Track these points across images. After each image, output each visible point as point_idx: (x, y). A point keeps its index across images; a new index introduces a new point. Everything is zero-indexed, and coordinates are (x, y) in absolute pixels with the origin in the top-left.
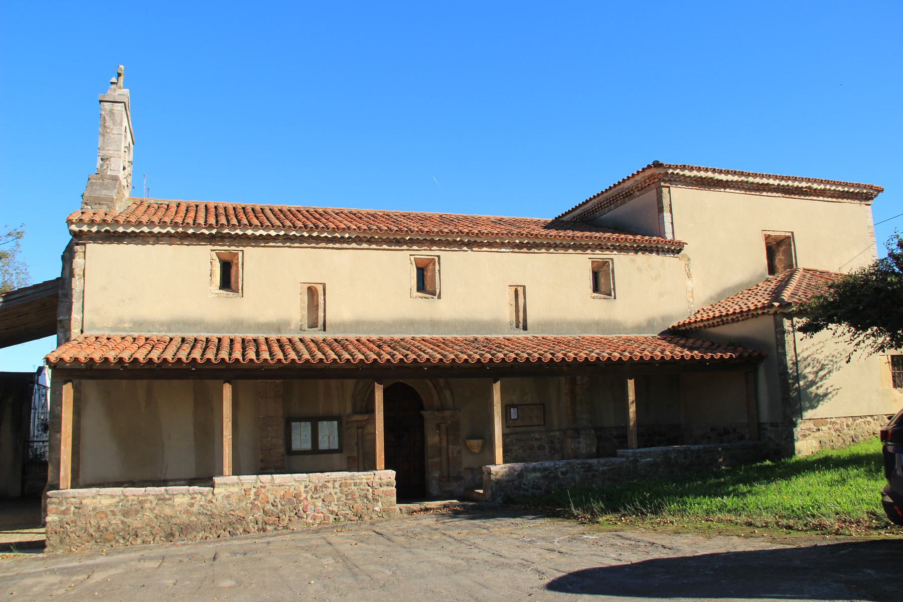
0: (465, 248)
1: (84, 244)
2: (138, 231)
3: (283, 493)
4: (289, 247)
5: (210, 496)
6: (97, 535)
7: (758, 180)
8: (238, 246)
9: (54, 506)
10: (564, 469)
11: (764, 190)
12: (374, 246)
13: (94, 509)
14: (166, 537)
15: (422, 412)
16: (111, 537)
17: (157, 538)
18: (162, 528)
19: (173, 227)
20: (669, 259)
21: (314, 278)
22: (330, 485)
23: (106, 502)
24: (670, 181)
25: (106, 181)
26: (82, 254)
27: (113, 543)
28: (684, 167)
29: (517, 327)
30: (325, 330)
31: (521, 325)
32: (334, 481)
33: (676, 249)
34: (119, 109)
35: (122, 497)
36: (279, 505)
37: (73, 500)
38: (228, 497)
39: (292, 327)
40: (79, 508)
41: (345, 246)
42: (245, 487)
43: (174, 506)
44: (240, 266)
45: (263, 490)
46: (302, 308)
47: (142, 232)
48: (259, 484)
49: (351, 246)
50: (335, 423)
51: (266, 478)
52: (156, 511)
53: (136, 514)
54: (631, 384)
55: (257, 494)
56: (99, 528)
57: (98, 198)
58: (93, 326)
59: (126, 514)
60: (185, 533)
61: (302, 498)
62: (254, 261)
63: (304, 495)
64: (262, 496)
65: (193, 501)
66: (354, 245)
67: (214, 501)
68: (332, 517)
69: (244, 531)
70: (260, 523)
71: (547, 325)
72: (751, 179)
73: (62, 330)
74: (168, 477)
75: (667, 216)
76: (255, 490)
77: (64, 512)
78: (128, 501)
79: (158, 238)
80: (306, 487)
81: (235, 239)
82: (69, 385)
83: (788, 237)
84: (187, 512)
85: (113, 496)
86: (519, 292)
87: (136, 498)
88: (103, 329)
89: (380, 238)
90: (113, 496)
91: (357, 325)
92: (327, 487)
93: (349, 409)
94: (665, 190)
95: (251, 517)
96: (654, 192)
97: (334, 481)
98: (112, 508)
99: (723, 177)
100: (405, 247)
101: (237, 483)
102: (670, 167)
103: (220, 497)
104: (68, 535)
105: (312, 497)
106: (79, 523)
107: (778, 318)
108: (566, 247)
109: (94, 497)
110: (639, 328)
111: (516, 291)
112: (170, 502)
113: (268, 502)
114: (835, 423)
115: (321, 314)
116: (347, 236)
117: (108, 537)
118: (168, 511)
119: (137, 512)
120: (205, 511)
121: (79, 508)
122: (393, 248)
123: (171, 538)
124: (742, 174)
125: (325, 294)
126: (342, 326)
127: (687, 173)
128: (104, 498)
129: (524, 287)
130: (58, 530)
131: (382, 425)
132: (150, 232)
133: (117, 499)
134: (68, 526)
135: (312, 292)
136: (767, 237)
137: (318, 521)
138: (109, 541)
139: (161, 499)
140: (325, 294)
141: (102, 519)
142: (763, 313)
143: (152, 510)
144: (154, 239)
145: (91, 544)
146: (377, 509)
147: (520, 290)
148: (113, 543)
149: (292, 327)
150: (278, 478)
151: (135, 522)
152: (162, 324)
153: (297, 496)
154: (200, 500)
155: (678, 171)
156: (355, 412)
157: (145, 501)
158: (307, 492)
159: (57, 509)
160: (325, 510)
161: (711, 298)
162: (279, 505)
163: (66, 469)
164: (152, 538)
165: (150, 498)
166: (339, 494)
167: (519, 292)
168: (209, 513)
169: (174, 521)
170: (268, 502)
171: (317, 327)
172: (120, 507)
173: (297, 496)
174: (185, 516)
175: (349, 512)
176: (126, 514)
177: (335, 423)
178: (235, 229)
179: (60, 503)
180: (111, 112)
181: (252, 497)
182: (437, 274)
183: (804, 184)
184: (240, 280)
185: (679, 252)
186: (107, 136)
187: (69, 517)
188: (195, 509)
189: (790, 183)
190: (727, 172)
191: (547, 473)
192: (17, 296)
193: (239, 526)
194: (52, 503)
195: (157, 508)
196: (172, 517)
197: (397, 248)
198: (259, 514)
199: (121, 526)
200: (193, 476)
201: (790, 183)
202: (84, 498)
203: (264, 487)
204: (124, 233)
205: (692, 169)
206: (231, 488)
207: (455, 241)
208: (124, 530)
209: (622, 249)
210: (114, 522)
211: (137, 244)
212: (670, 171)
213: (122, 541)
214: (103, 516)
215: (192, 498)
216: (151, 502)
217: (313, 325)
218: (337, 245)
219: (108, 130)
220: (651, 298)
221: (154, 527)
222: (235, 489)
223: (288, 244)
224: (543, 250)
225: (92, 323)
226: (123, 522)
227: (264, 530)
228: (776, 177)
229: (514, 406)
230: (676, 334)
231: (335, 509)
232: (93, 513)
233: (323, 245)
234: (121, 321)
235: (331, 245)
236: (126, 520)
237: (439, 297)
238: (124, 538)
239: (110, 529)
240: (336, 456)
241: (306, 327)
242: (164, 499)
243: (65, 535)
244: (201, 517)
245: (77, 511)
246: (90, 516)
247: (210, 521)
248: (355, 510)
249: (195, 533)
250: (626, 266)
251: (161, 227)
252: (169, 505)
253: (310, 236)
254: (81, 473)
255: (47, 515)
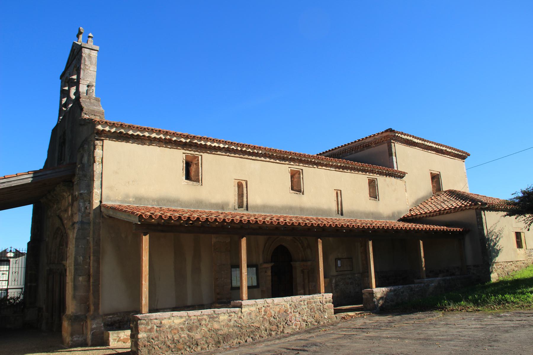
0: (315, 166)
1: (103, 140)
2: (141, 135)
3: (278, 310)
4: (228, 156)
5: (240, 314)
6: (172, 346)
7: (428, 144)
8: (200, 152)
9: (143, 326)
10: (402, 290)
11: (429, 150)
12: (272, 160)
13: (170, 327)
14: (216, 344)
15: (292, 263)
16: (181, 346)
17: (210, 346)
18: (213, 338)
19: (164, 135)
20: (398, 181)
21: (242, 177)
22: (302, 303)
23: (177, 321)
24: (395, 140)
25: (92, 101)
26: (101, 147)
27: (183, 351)
28: (402, 133)
29: (338, 213)
30: (247, 210)
31: (340, 212)
32: (304, 301)
33: (400, 175)
34: (95, 54)
35: (187, 317)
36: (278, 318)
37: (155, 321)
38: (250, 314)
39: (230, 207)
40: (160, 327)
41: (258, 158)
42: (258, 307)
43: (219, 322)
44: (200, 165)
45: (268, 308)
46: (235, 195)
47: (144, 136)
48: (266, 304)
49: (260, 159)
50: (255, 269)
51: (269, 300)
52: (209, 326)
53: (197, 329)
54: (421, 242)
55: (265, 312)
56: (173, 340)
57: (93, 111)
58: (108, 198)
59: (190, 329)
60: (226, 340)
61: (289, 313)
62: (208, 162)
63: (290, 310)
64: (268, 312)
65: (230, 318)
66: (262, 159)
67: (242, 317)
68: (305, 324)
69: (260, 336)
70: (268, 330)
71: (352, 213)
72: (426, 143)
73: (82, 201)
74: (159, 307)
75: (394, 157)
76: (264, 308)
77: (150, 330)
78: (191, 320)
79: (151, 141)
80: (290, 305)
81: (198, 147)
82: (148, 236)
83: (438, 175)
84: (227, 325)
85: (181, 317)
86: (338, 193)
87: (196, 317)
88: (115, 201)
89: (272, 155)
90: (181, 317)
91: (264, 207)
92: (301, 305)
93: (261, 261)
94: (393, 144)
95: (263, 327)
96: (385, 145)
97: (304, 301)
98: (181, 326)
99: (416, 140)
100: (287, 162)
101: (255, 304)
102: (397, 133)
103: (245, 314)
104: (153, 347)
105: (294, 312)
106: (160, 338)
107: (478, 211)
108: (358, 170)
109: (169, 318)
110: (389, 218)
111: (337, 193)
112: (217, 319)
113: (271, 316)
114: (501, 265)
115: (245, 200)
116: (260, 152)
117: (180, 347)
118: (216, 326)
119: (197, 327)
120: (237, 325)
121: (160, 327)
122: (281, 162)
123: (219, 345)
124: (423, 140)
125: (247, 187)
126: (257, 208)
127: (403, 136)
128: (174, 319)
129: (341, 191)
130: (147, 343)
131: (322, 265)
132: (149, 137)
133: (184, 319)
134: (153, 340)
135: (240, 186)
136: (431, 173)
137: (298, 327)
138: (180, 350)
139: (211, 317)
140: (247, 187)
141: (175, 334)
142: (469, 209)
143: (206, 326)
144: (149, 141)
145: (168, 353)
146: (326, 317)
147: (339, 192)
148: (183, 351)
149: (230, 207)
150: (277, 300)
151: (197, 335)
152: (153, 200)
153: (285, 312)
154: (234, 317)
155: (399, 135)
156: (265, 262)
157: (202, 319)
158: (291, 308)
159: (145, 328)
160: (300, 320)
161: (413, 203)
162: (278, 318)
163: (146, 298)
164: (206, 345)
165: (205, 317)
166: (307, 309)
167: (338, 193)
168: (240, 325)
169: (220, 332)
170: (271, 316)
171: (242, 207)
172: (186, 325)
173: (285, 312)
174: (226, 329)
175: (313, 320)
176: (190, 329)
177: (255, 269)
178: (200, 141)
179: (147, 324)
180: (89, 55)
181: (263, 313)
182: (302, 180)
183: (444, 148)
184: (200, 174)
185: (403, 177)
186: (86, 72)
187: (154, 334)
188: (232, 323)
189: (439, 147)
190: (418, 139)
191: (396, 292)
192: (40, 174)
193: (257, 333)
194: (142, 324)
195: (209, 324)
196: (218, 330)
197: (283, 162)
198: (267, 325)
199: (187, 338)
200: (174, 306)
201: (439, 147)
202: (163, 319)
203: (269, 306)
204: (132, 135)
205: (405, 135)
206: (252, 309)
207: (311, 161)
208: (189, 341)
209: (381, 174)
210: (183, 335)
211: (138, 144)
212: (397, 134)
213: (188, 349)
214: (176, 332)
215: (229, 316)
216: (206, 320)
217: (240, 206)
218: (254, 158)
219: (87, 67)
220: (396, 199)
221: (207, 338)
222: (253, 309)
223: (228, 154)
224: (349, 171)
225: (108, 196)
226: (188, 335)
227: (271, 335)
228: (435, 144)
229: (339, 259)
230: (405, 220)
231: (306, 318)
232: (169, 330)
233: (246, 156)
234: (127, 196)
235: (250, 157)
236: (190, 334)
237: (303, 194)
238: (190, 347)
239: (181, 341)
240: (255, 290)
241: (237, 207)
242: (213, 318)
243: (151, 348)
244: (235, 329)
245: (158, 329)
246: (167, 332)
247: (240, 331)
248: (315, 318)
249: (232, 340)
250: (384, 183)
251: (157, 134)
252: (217, 321)
253: (241, 150)
254: (100, 306)
255: (138, 333)
